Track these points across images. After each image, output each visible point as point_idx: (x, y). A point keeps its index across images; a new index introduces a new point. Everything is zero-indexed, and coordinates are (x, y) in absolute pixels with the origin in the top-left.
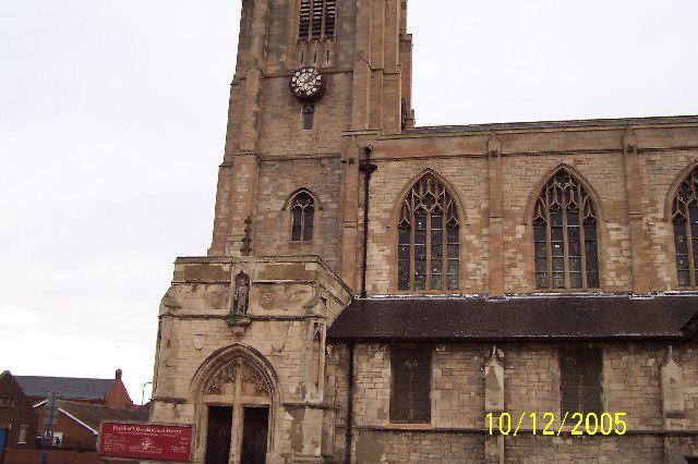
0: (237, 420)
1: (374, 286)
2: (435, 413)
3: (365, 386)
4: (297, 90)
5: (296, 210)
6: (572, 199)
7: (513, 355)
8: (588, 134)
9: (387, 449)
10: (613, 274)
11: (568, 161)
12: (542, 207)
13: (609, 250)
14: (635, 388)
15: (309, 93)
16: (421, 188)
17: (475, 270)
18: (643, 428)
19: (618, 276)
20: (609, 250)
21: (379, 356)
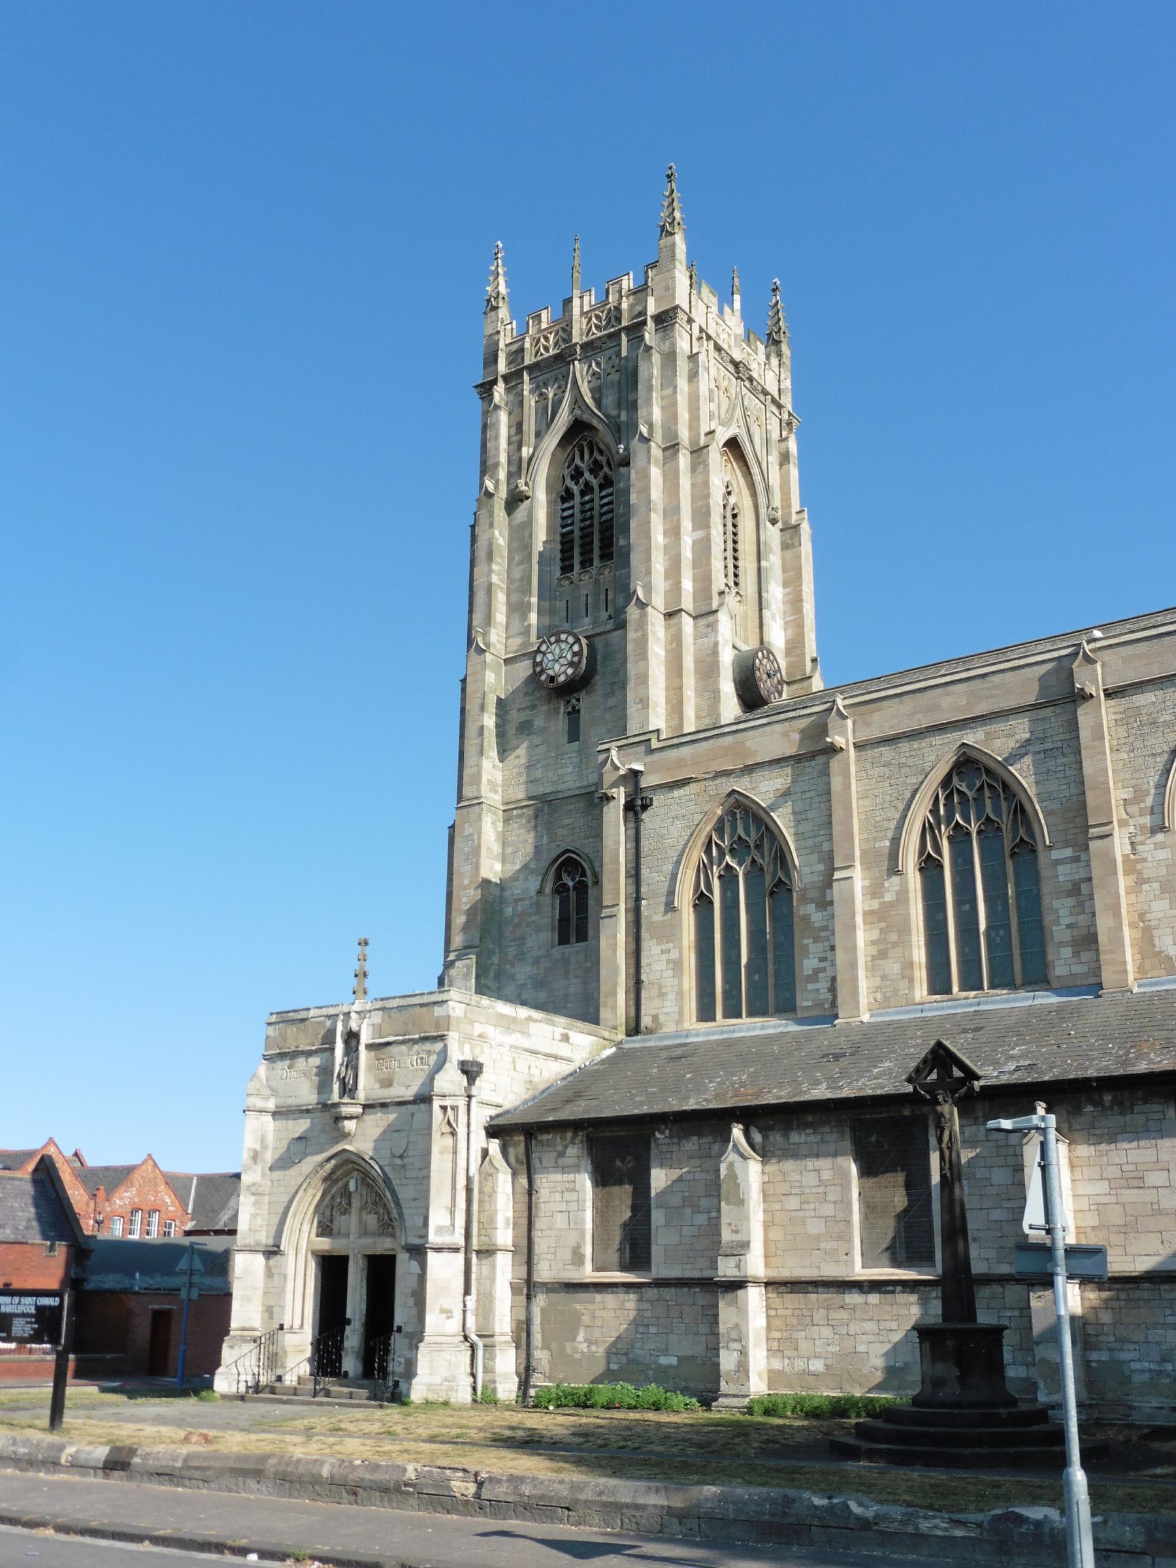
0: (202, 1293)
1: (655, 1018)
2: (656, 1251)
3: (810, 1179)
4: (543, 677)
5: (560, 889)
6: (989, 810)
7: (777, 1137)
8: (1009, 674)
9: (586, 1319)
10: (1067, 952)
11: (972, 737)
12: (707, 876)
13: (1056, 904)
14: (989, 1190)
15: (562, 678)
16: (727, 829)
17: (817, 971)
18: (1004, 1269)
19: (1076, 954)
20: (1056, 904)
21: (573, 1151)
